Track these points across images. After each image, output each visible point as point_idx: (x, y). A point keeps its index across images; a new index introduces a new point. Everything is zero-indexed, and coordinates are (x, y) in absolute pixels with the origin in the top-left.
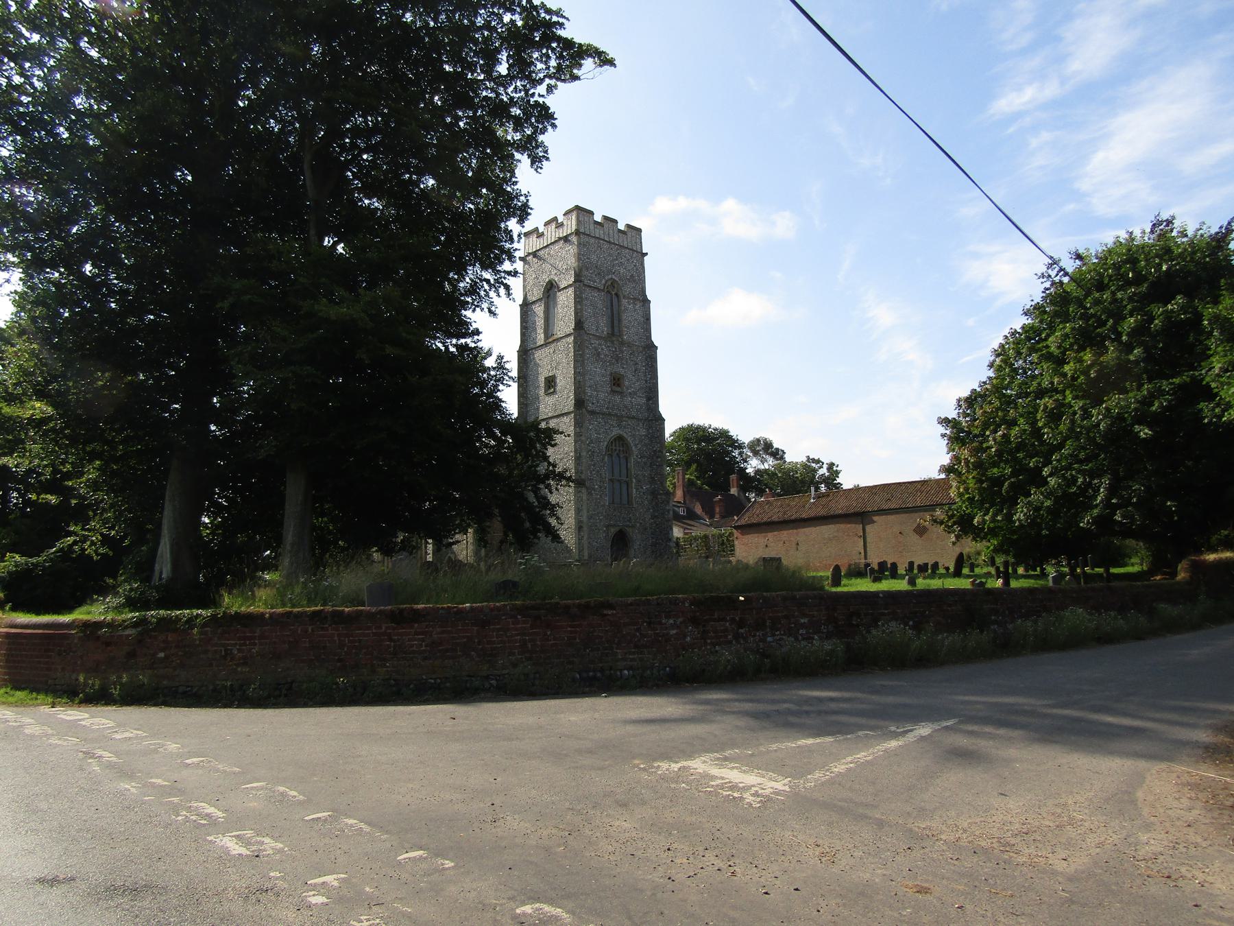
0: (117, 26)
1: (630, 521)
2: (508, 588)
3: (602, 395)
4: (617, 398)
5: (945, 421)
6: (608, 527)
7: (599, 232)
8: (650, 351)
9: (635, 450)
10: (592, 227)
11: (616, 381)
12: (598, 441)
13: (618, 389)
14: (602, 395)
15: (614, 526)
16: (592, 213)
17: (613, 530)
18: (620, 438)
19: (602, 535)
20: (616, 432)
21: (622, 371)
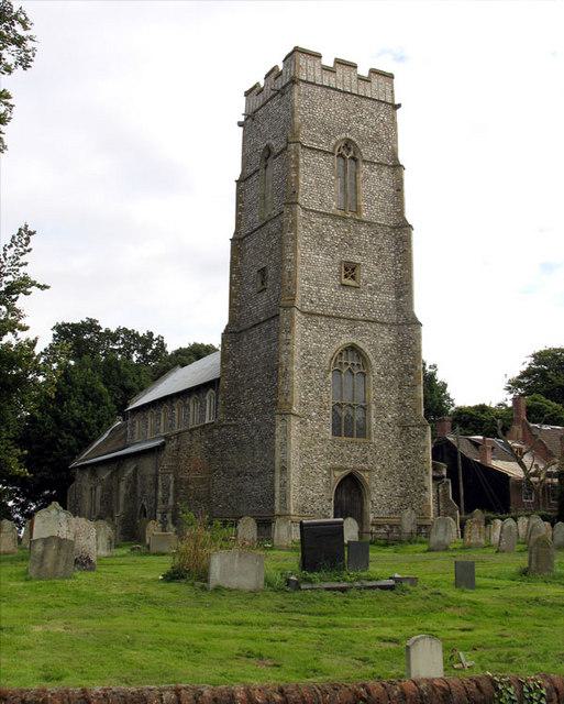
0: (497, 417)
1: (365, 460)
2: (129, 595)
3: (325, 292)
4: (350, 294)
5: (240, 124)
6: (332, 469)
7: (328, 80)
8: (401, 231)
9: (376, 366)
10: (354, 83)
11: (350, 270)
12: (318, 352)
13: (351, 282)
14: (325, 292)
15: (339, 469)
16: (355, 66)
17: (339, 475)
18: (352, 348)
19: (321, 488)
20: (346, 340)
21: (358, 259)
